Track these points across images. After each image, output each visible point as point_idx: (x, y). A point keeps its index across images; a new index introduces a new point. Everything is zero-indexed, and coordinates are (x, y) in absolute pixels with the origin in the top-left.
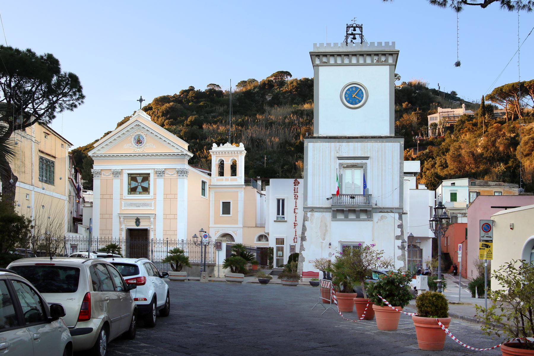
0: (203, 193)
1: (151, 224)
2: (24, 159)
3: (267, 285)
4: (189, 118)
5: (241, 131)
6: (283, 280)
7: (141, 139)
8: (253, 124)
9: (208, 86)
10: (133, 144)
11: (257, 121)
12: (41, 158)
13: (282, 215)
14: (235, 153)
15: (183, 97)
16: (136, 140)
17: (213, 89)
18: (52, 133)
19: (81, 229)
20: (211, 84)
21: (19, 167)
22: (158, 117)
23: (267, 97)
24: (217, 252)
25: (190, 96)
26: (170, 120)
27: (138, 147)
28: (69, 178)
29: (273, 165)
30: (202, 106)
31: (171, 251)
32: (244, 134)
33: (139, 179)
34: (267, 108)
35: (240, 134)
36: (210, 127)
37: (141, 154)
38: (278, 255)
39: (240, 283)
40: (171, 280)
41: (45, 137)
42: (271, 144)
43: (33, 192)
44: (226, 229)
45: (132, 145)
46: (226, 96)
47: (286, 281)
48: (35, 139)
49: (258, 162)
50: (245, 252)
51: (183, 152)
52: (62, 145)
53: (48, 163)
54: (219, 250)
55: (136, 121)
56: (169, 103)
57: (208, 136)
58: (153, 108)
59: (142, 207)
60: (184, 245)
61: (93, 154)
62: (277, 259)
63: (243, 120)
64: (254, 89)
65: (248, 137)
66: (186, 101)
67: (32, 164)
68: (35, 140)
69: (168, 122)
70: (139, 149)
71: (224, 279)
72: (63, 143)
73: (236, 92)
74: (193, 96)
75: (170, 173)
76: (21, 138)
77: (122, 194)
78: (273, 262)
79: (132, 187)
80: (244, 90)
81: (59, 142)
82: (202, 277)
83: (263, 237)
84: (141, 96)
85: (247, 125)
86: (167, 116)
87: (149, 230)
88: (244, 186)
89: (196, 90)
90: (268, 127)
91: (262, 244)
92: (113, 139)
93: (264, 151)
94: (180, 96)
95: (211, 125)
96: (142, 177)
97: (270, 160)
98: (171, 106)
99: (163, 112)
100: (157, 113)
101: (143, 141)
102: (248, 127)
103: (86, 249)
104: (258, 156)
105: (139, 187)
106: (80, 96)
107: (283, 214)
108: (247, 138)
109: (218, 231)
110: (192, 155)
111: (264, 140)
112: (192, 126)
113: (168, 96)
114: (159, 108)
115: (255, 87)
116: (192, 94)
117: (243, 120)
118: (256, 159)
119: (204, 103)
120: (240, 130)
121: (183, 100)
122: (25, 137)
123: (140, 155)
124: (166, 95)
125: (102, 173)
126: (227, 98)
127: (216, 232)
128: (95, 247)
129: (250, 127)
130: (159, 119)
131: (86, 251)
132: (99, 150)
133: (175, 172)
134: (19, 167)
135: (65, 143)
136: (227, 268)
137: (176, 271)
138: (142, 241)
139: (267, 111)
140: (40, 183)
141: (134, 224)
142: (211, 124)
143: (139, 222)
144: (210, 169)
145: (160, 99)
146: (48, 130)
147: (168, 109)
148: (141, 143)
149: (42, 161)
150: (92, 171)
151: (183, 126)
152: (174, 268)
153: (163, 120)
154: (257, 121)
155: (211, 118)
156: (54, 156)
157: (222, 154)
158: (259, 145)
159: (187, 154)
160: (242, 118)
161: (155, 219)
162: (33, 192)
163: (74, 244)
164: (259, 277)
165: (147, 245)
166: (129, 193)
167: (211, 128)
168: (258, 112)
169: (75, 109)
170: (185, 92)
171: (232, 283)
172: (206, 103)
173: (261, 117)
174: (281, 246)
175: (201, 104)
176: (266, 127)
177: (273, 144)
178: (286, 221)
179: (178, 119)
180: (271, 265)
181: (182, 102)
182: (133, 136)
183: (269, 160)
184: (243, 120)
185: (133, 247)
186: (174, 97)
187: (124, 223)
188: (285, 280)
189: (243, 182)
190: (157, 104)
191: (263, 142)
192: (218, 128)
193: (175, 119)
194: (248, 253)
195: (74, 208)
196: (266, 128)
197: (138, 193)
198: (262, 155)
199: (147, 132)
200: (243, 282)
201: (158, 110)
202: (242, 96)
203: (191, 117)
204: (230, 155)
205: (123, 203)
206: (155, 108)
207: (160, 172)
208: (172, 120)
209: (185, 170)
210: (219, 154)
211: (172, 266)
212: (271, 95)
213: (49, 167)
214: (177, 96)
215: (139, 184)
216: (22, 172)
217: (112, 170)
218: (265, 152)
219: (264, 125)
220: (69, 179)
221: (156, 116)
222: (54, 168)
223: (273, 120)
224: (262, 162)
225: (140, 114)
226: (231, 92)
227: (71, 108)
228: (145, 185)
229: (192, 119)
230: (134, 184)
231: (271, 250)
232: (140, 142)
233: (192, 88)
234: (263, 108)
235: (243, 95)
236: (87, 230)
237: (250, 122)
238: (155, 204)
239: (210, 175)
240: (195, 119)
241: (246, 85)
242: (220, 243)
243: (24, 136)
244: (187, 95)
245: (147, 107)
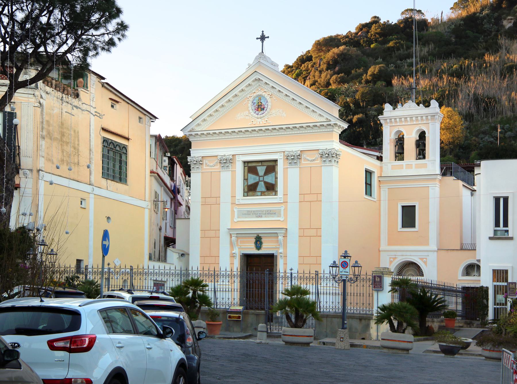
0: (369, 191)
1: (279, 245)
2: (77, 143)
3: (456, 356)
4: (370, 69)
5: (457, 85)
6: (484, 348)
7: (263, 103)
8: (478, 71)
9: (403, 13)
10: (251, 111)
11: (486, 66)
12: (105, 140)
13: (504, 226)
14: (422, 120)
15: (362, 36)
16: (255, 105)
17: (411, 17)
18: (124, 100)
19: (172, 254)
20: (407, 10)
21: (70, 155)
22: (321, 72)
23: (505, 23)
24: (375, 294)
25: (372, 33)
26: (339, 76)
27: (259, 116)
28: (152, 172)
29: (513, 142)
30: (393, 47)
31: (287, 290)
32: (461, 90)
33: (261, 170)
34: (503, 41)
35: (456, 91)
36: (404, 82)
37: (263, 128)
38: (497, 301)
39: (405, 352)
40: (287, 343)
41: (112, 106)
42: (511, 104)
43: (92, 196)
44: (408, 253)
45: (250, 113)
46: (433, 27)
47: (490, 350)
48: (95, 110)
49: (487, 138)
50: (429, 294)
51: (330, 121)
52: (140, 118)
53: (118, 148)
54: (378, 291)
55: (255, 73)
56: (338, 48)
57: (401, 98)
58: (314, 57)
59: (266, 217)
60: (319, 281)
61: (190, 131)
62: (495, 308)
63: (461, 65)
64: (482, 10)
65: (469, 95)
66: (367, 41)
67: (90, 150)
68: (96, 112)
69: (336, 78)
70: (259, 120)
71: (378, 344)
72: (142, 116)
73: (450, 20)
74: (377, 33)
75: (308, 158)
76: (73, 109)
77: (233, 197)
78: (487, 314)
79: (249, 184)
80: (464, 14)
81: (136, 114)
82: (338, 338)
83: (474, 269)
84: (263, 31)
85: (468, 74)
86: (335, 68)
87: (277, 256)
88: (440, 177)
89: (382, 22)
90: (505, 76)
91: (470, 281)
92: (220, 105)
93: (497, 117)
94: (356, 34)
95: (405, 79)
96: (265, 167)
97: (509, 133)
98: (340, 51)
99: (328, 63)
100: (320, 65)
101: (266, 106)
102: (469, 77)
103: (118, 286)
104: (486, 128)
105: (260, 183)
106: (120, 27)
107: (506, 224)
108: (467, 97)
109: (394, 257)
110: (345, 126)
111: (498, 98)
112: (375, 83)
113: (338, 35)
114: (322, 57)
115: (483, 8)
116: (376, 30)
117: (461, 67)
118: (484, 133)
119: (396, 43)
120: (456, 84)
121: (362, 41)
122: (80, 108)
123: (261, 130)
124: (333, 34)
125: (205, 161)
126: (434, 30)
127: (392, 259)
128: (227, 286)
129: (472, 78)
130: (322, 75)
131: (118, 289)
132: (199, 125)
133: (317, 156)
134: (69, 156)
135: (145, 115)
136: (112, 320)
137: (296, 327)
138: (256, 274)
139: (504, 47)
140: (104, 181)
141: (253, 245)
142: (405, 76)
143: (261, 243)
144: (380, 150)
145: (322, 40)
146: (116, 95)
147: (336, 57)
148: (263, 109)
149: (106, 145)
150: (189, 160)
151: (360, 83)
152: (291, 321)
153: (329, 76)
154: (486, 66)
155: (406, 67)
156: (127, 136)
157: (401, 121)
158: (488, 108)
159: (336, 124)
160: (459, 62)
161: (285, 236)
162: (92, 196)
163: (161, 281)
164: (440, 342)
165: (272, 283)
166: (246, 194)
167: (406, 83)
168: (487, 50)
169: (113, 49)
170: (365, 27)
171: (391, 351)
172: (399, 43)
173: (492, 58)
174: (498, 284)
175: (391, 44)
176: (501, 74)
177: (513, 105)
178: (511, 238)
179: (353, 72)
180: (484, 319)
181: (360, 44)
182: (251, 99)
183: (506, 132)
184: (461, 65)
185: (253, 285)
186: (346, 37)
187: (238, 245)
188: (489, 348)
189: (438, 171)
190: (319, 50)
191: (496, 103)
192: (417, 84)
193: (348, 73)
194: (433, 297)
195: (168, 221)
196: (501, 77)
197: (259, 194)
198: (493, 125)
199: (273, 91)
200: (411, 349)
201: (321, 59)
202: (460, 24)
203: (372, 67)
204: (415, 123)
205: (235, 210)
206: (316, 57)
207: (293, 157)
208: (343, 75)
209: (333, 151)
210: (396, 122)
211: (288, 318)
212: (512, 19)
213: (118, 155)
214: (351, 35)
215: (261, 179)
216: (75, 164)
217: (219, 157)
218: (499, 119)
219: (499, 73)
220: (153, 174)
221: (317, 70)
222: (126, 157)
223: (514, 62)
224: (493, 137)
225: (261, 61)
226: (441, 20)
227: (106, 47)
228: (270, 179)
229: (374, 71)
230: (252, 179)
231: (484, 291)
232: (262, 107)
233: (376, 19)
234: (496, 43)
235: (462, 22)
236: (181, 258)
237: (473, 68)
238: (286, 210)
239: (380, 159)
240: (380, 71)
241: (467, 6)
242: (380, 277)
243: (78, 105)
244: (368, 32)
245: (304, 57)
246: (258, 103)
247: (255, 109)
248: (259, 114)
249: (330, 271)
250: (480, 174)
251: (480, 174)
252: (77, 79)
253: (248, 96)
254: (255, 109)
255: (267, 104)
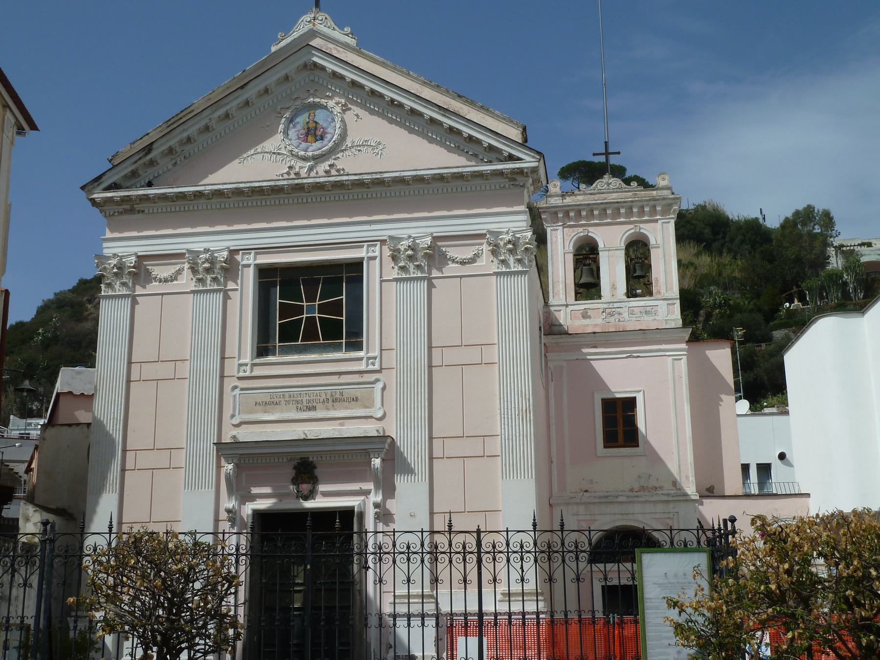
148: (322, 138)
246: (307, 123)
247: (299, 138)
248: (311, 149)
249: (111, 522)
250: (619, 153)
251: (619, 153)
252: (769, 323)
253: (279, 107)
254: (299, 138)
255: (333, 124)
